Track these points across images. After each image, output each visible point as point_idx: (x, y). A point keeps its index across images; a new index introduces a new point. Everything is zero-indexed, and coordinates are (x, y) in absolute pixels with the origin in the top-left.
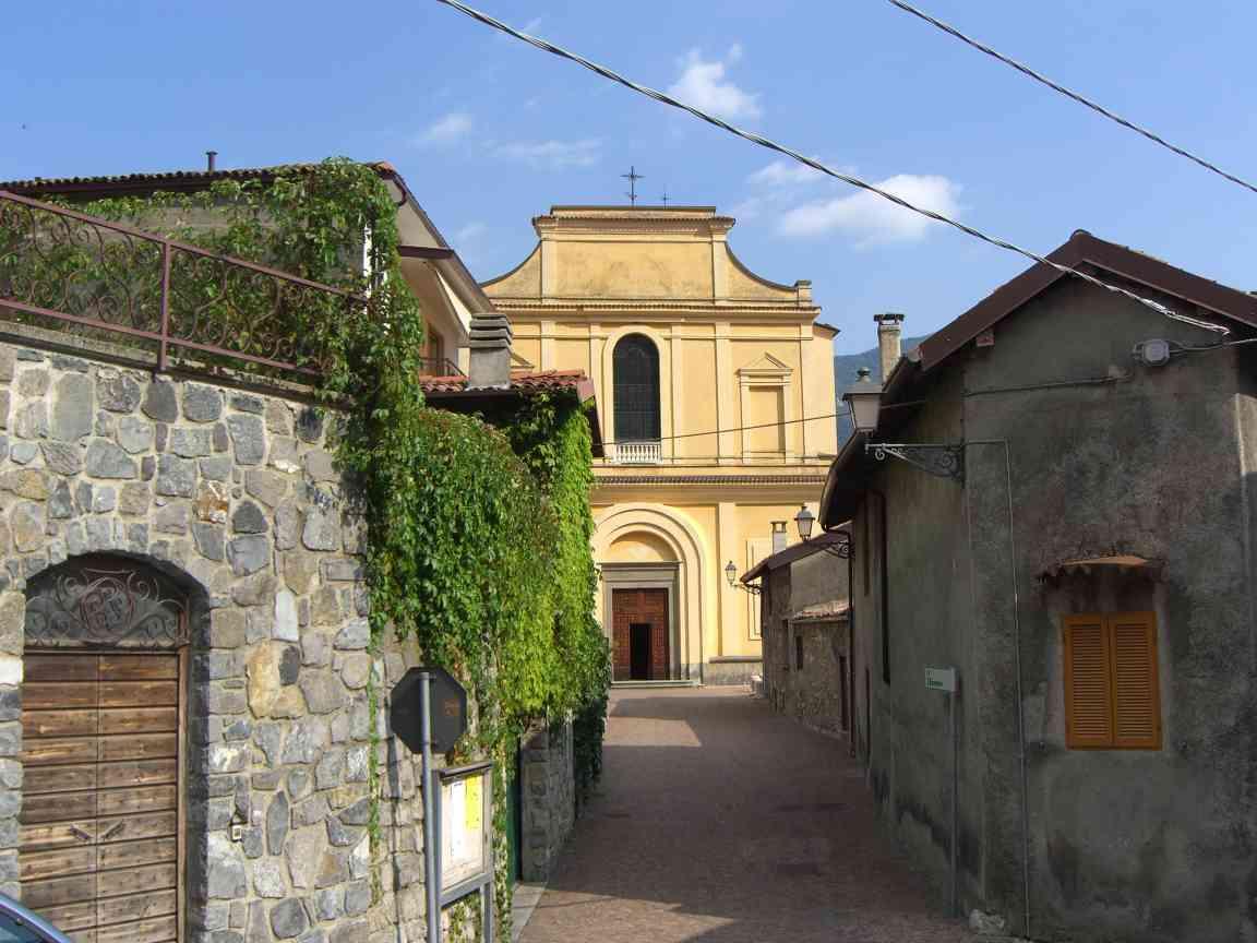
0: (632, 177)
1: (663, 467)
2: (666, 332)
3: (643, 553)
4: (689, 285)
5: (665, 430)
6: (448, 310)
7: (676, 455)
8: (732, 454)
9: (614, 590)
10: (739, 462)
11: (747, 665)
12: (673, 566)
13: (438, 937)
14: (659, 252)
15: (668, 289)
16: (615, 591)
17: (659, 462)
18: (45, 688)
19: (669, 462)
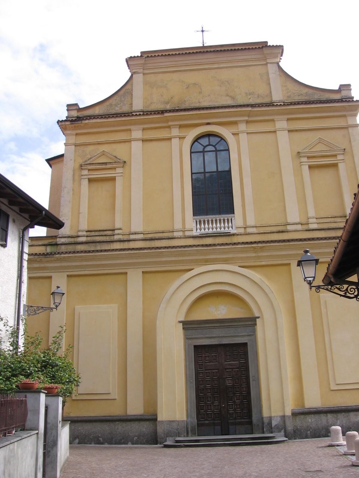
0: (203, 31)
1: (238, 235)
2: (234, 129)
3: (220, 311)
4: (250, 94)
5: (246, 342)
6: (148, 139)
7: (249, 223)
8: (298, 220)
9: (195, 347)
10: (305, 227)
11: (329, 416)
12: (251, 322)
13: (271, 63)
14: (225, 75)
15: (233, 98)
16: (197, 348)
17: (233, 231)
18: (341, 107)
19: (242, 231)
